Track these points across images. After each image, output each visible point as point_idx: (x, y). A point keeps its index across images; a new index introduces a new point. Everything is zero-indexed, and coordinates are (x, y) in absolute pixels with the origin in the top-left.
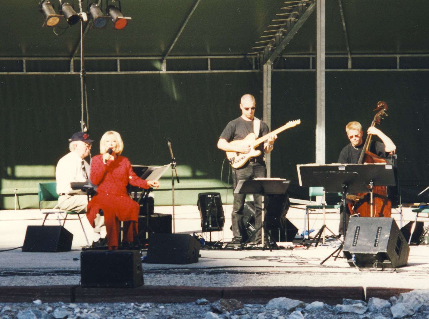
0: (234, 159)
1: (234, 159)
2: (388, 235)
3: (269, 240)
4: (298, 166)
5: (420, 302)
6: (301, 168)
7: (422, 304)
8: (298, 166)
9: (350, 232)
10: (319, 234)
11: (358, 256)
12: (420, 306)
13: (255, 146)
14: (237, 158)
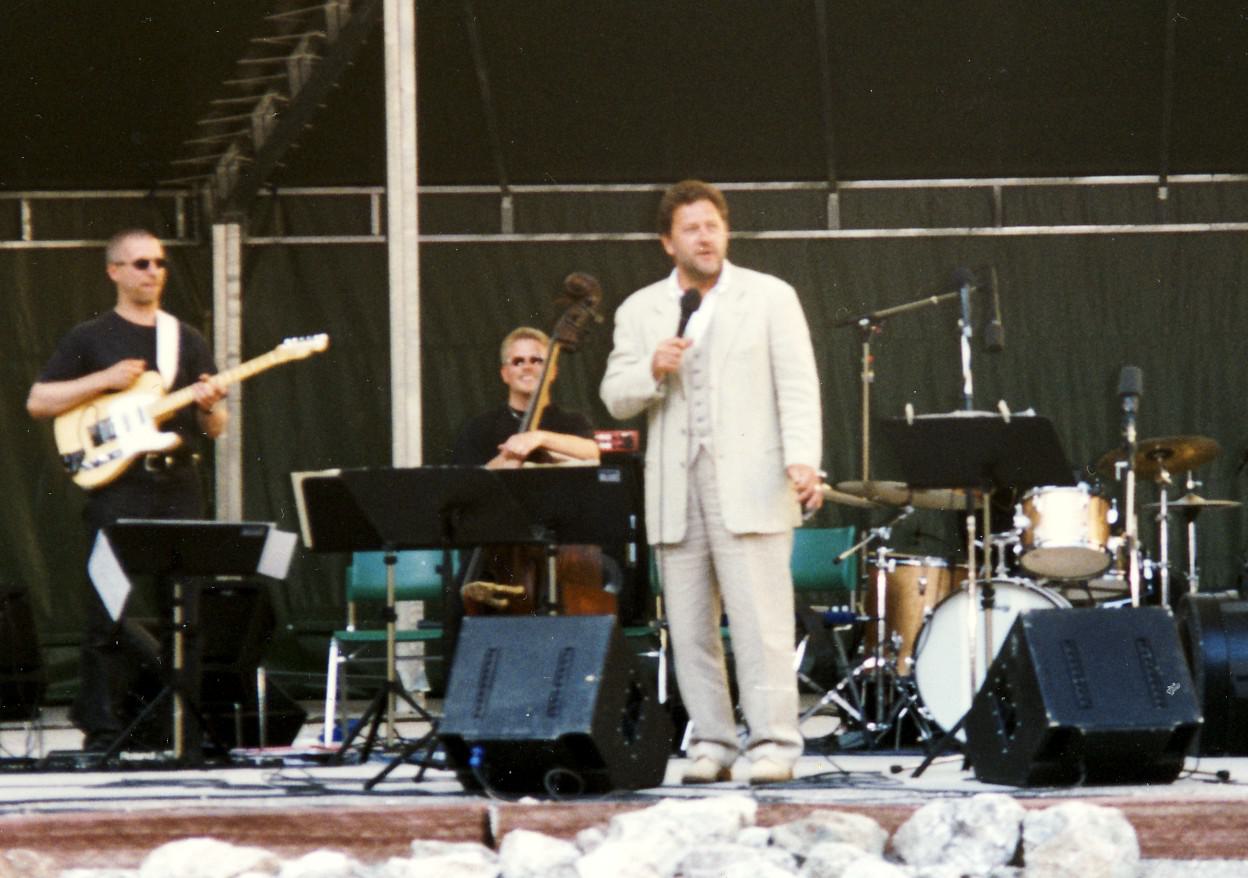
0: (80, 456)
1: (80, 456)
2: (596, 675)
3: (173, 628)
4: (298, 478)
5: (681, 843)
6: (308, 485)
7: (689, 849)
8: (298, 478)
9: (463, 674)
10: (372, 718)
11: (495, 750)
12: (680, 855)
13: (161, 416)
14: (93, 454)
